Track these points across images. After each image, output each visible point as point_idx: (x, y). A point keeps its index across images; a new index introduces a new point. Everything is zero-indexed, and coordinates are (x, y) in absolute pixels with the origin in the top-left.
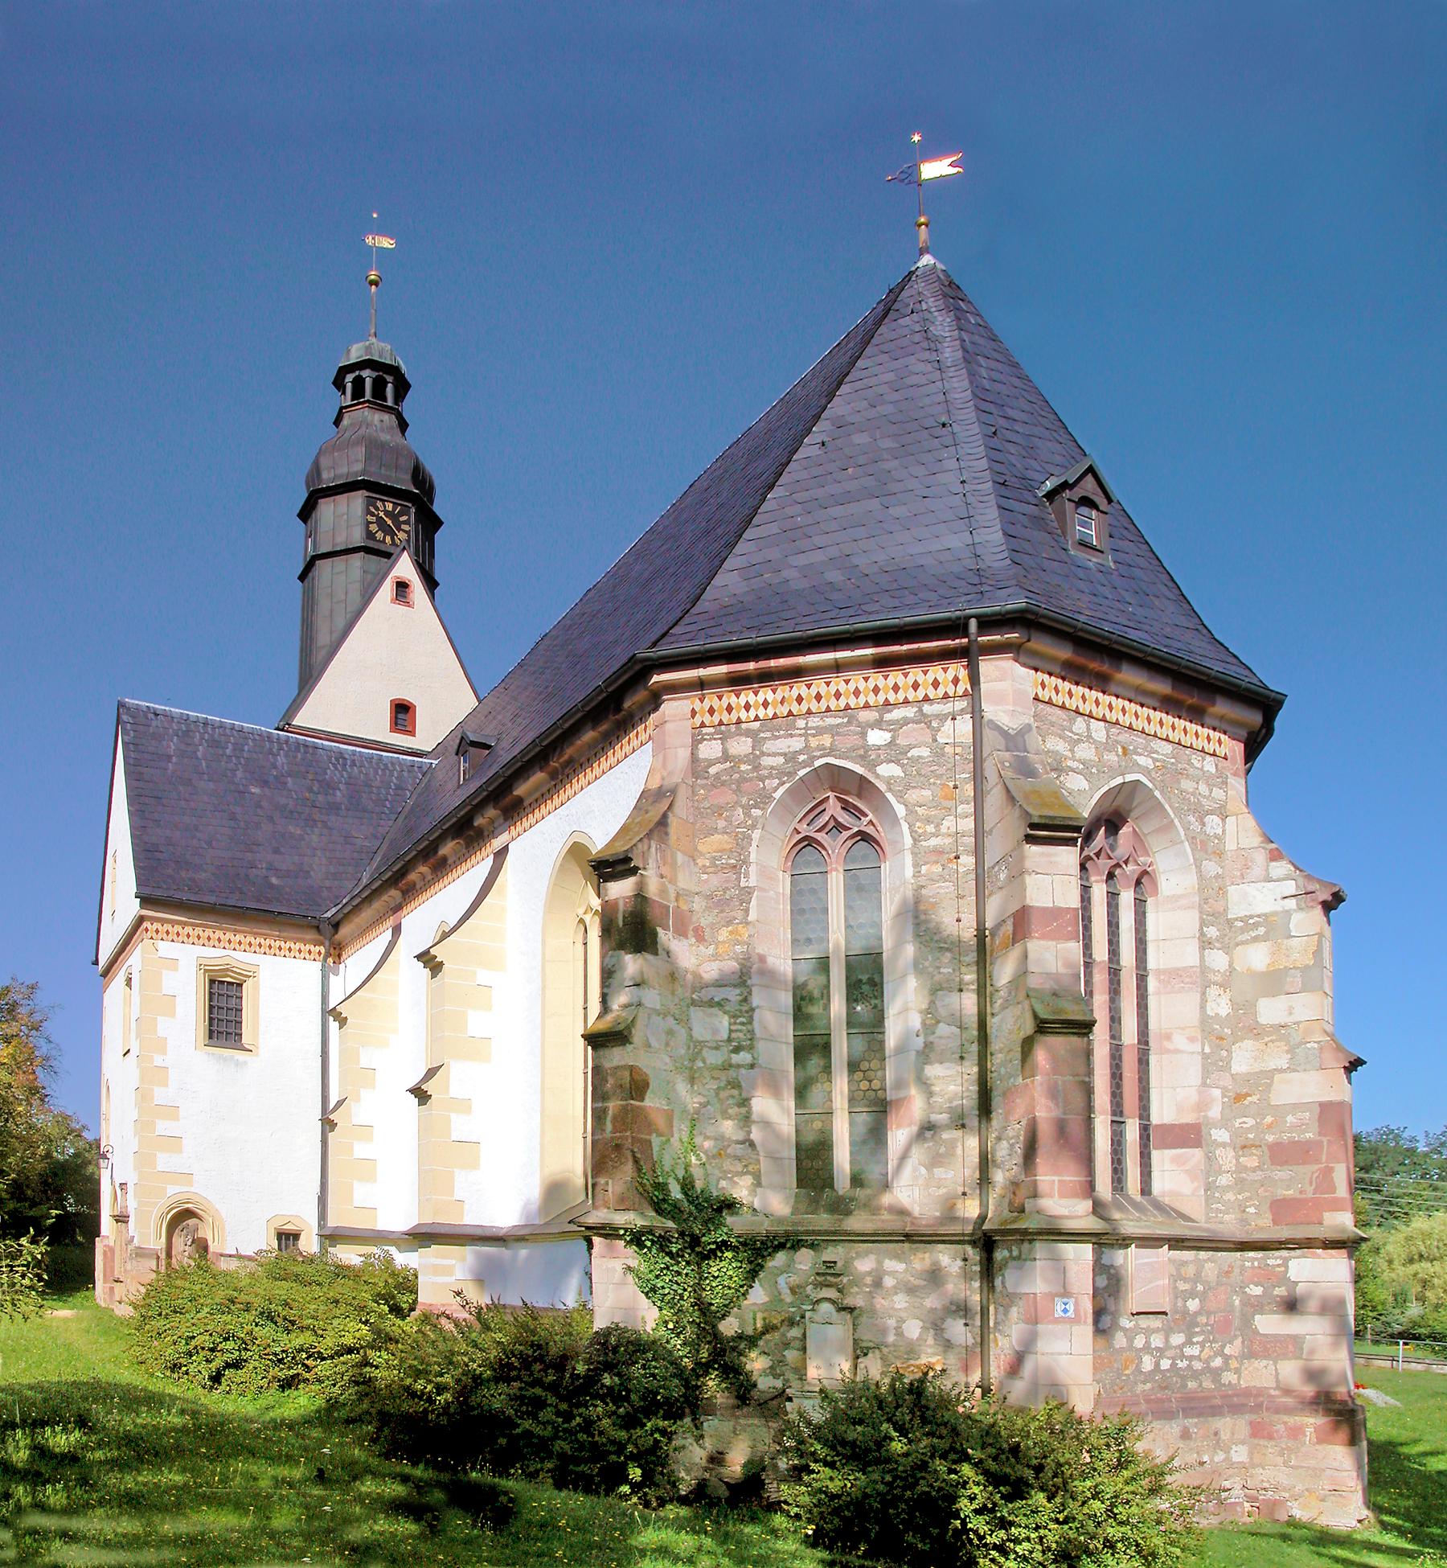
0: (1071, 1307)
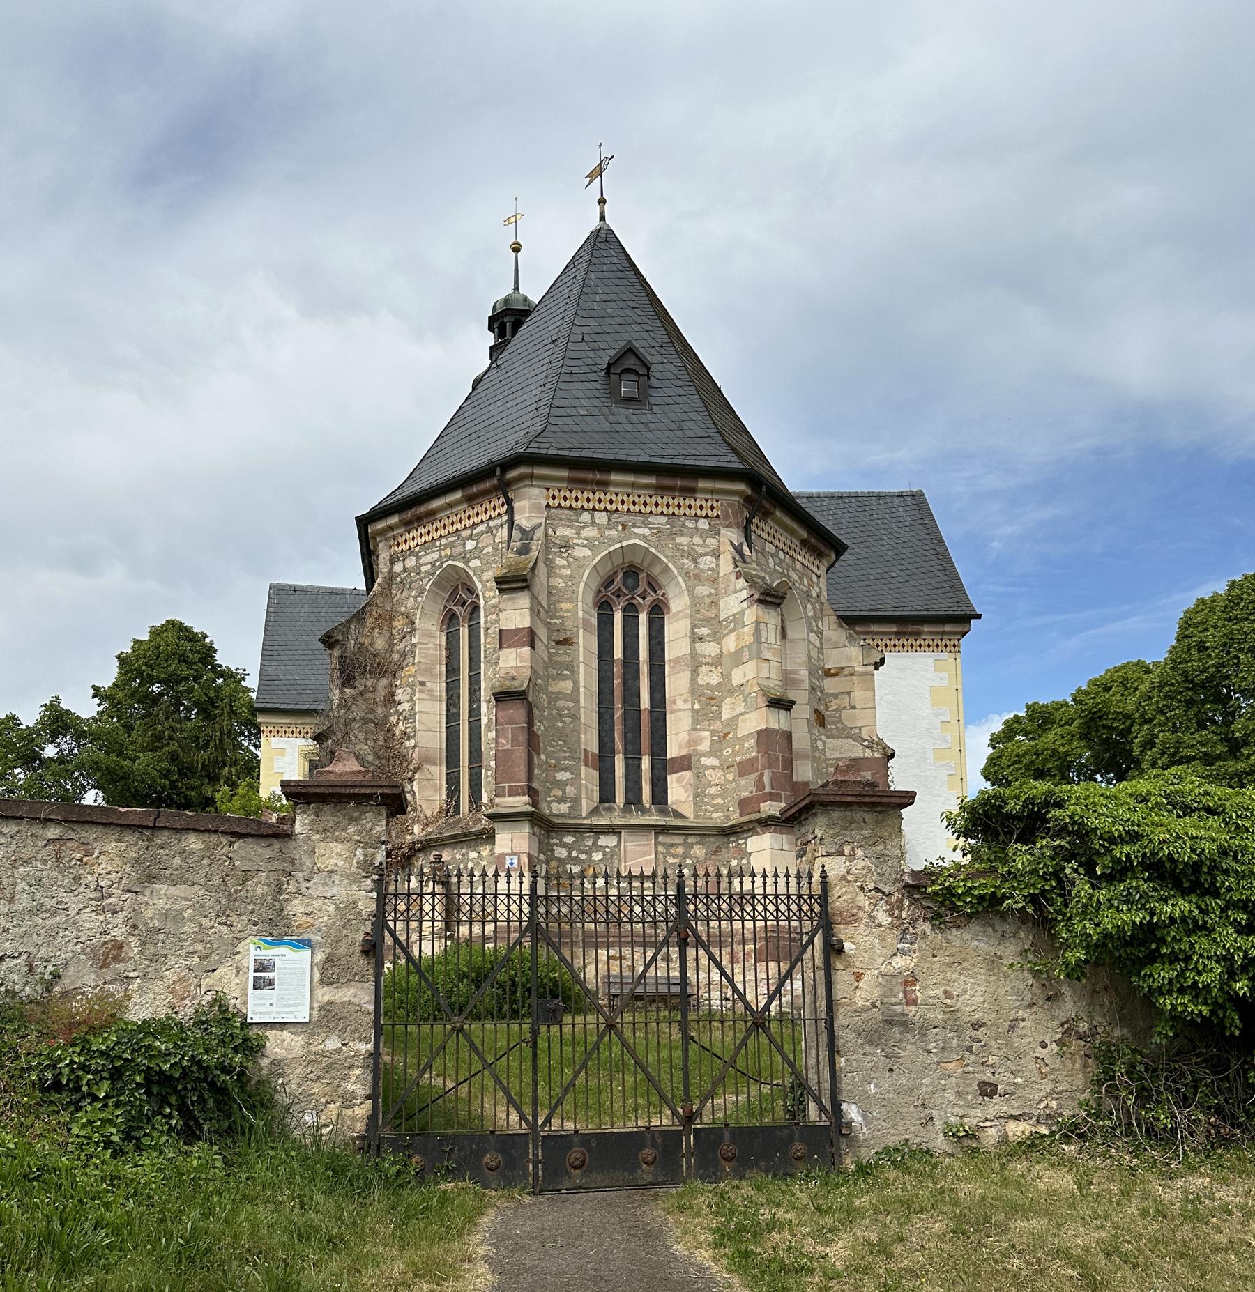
0: (515, 861)
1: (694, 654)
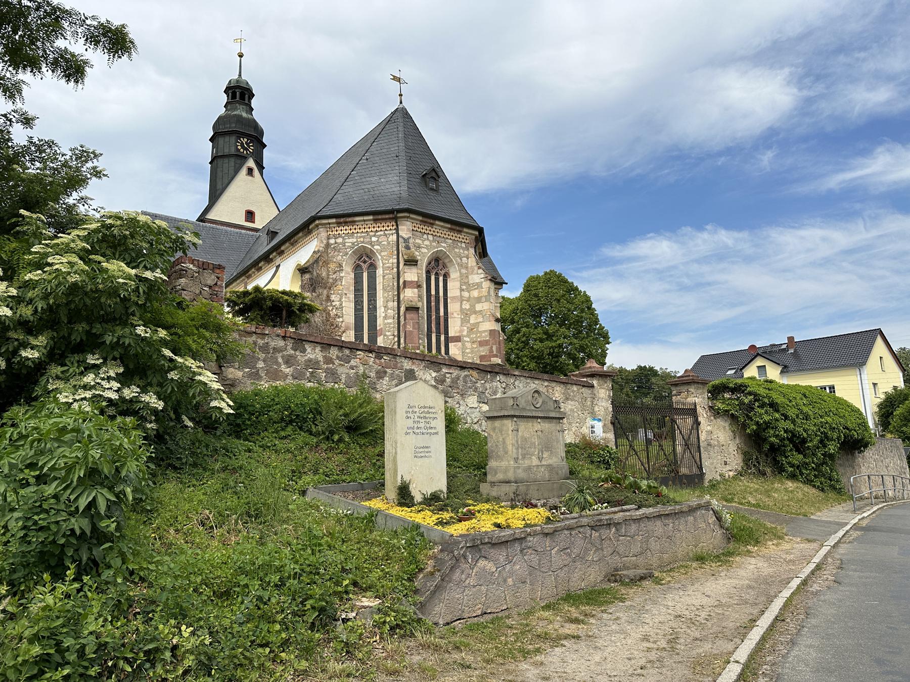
1: (461, 296)
